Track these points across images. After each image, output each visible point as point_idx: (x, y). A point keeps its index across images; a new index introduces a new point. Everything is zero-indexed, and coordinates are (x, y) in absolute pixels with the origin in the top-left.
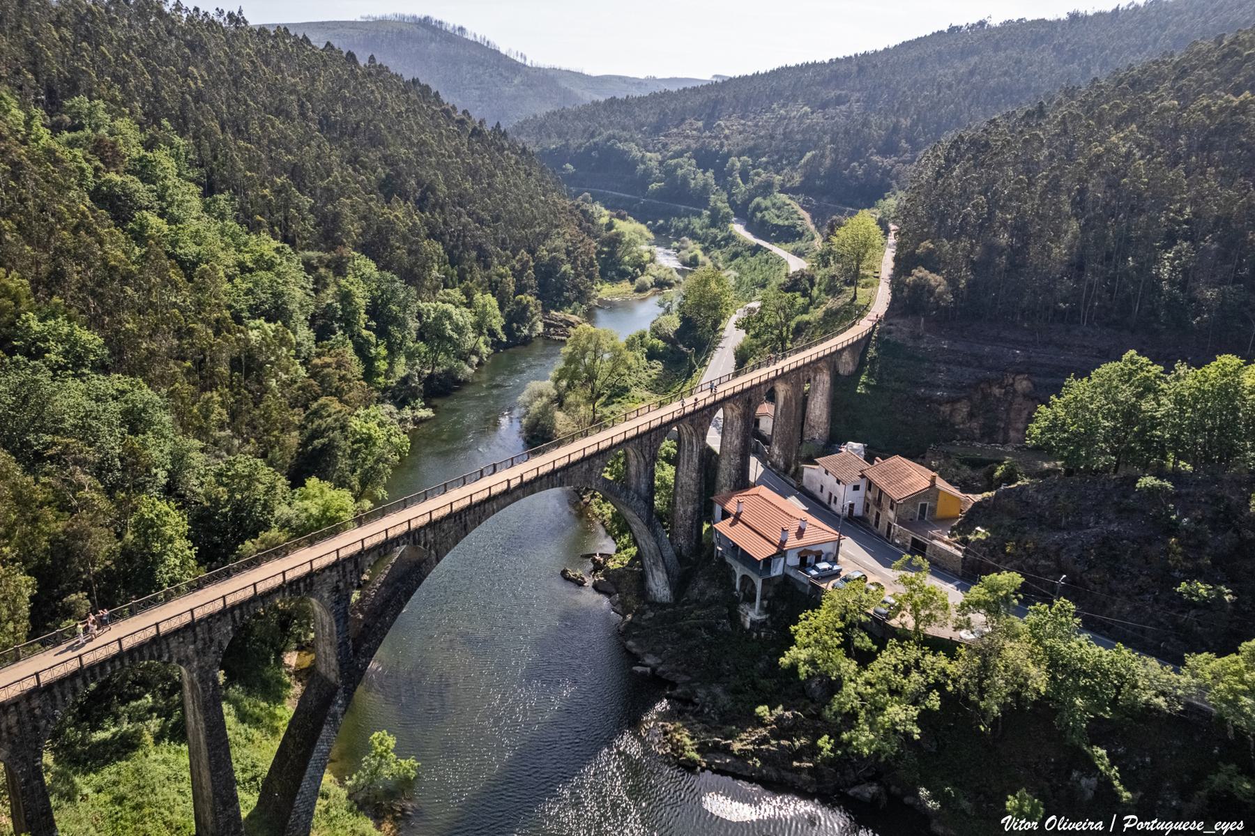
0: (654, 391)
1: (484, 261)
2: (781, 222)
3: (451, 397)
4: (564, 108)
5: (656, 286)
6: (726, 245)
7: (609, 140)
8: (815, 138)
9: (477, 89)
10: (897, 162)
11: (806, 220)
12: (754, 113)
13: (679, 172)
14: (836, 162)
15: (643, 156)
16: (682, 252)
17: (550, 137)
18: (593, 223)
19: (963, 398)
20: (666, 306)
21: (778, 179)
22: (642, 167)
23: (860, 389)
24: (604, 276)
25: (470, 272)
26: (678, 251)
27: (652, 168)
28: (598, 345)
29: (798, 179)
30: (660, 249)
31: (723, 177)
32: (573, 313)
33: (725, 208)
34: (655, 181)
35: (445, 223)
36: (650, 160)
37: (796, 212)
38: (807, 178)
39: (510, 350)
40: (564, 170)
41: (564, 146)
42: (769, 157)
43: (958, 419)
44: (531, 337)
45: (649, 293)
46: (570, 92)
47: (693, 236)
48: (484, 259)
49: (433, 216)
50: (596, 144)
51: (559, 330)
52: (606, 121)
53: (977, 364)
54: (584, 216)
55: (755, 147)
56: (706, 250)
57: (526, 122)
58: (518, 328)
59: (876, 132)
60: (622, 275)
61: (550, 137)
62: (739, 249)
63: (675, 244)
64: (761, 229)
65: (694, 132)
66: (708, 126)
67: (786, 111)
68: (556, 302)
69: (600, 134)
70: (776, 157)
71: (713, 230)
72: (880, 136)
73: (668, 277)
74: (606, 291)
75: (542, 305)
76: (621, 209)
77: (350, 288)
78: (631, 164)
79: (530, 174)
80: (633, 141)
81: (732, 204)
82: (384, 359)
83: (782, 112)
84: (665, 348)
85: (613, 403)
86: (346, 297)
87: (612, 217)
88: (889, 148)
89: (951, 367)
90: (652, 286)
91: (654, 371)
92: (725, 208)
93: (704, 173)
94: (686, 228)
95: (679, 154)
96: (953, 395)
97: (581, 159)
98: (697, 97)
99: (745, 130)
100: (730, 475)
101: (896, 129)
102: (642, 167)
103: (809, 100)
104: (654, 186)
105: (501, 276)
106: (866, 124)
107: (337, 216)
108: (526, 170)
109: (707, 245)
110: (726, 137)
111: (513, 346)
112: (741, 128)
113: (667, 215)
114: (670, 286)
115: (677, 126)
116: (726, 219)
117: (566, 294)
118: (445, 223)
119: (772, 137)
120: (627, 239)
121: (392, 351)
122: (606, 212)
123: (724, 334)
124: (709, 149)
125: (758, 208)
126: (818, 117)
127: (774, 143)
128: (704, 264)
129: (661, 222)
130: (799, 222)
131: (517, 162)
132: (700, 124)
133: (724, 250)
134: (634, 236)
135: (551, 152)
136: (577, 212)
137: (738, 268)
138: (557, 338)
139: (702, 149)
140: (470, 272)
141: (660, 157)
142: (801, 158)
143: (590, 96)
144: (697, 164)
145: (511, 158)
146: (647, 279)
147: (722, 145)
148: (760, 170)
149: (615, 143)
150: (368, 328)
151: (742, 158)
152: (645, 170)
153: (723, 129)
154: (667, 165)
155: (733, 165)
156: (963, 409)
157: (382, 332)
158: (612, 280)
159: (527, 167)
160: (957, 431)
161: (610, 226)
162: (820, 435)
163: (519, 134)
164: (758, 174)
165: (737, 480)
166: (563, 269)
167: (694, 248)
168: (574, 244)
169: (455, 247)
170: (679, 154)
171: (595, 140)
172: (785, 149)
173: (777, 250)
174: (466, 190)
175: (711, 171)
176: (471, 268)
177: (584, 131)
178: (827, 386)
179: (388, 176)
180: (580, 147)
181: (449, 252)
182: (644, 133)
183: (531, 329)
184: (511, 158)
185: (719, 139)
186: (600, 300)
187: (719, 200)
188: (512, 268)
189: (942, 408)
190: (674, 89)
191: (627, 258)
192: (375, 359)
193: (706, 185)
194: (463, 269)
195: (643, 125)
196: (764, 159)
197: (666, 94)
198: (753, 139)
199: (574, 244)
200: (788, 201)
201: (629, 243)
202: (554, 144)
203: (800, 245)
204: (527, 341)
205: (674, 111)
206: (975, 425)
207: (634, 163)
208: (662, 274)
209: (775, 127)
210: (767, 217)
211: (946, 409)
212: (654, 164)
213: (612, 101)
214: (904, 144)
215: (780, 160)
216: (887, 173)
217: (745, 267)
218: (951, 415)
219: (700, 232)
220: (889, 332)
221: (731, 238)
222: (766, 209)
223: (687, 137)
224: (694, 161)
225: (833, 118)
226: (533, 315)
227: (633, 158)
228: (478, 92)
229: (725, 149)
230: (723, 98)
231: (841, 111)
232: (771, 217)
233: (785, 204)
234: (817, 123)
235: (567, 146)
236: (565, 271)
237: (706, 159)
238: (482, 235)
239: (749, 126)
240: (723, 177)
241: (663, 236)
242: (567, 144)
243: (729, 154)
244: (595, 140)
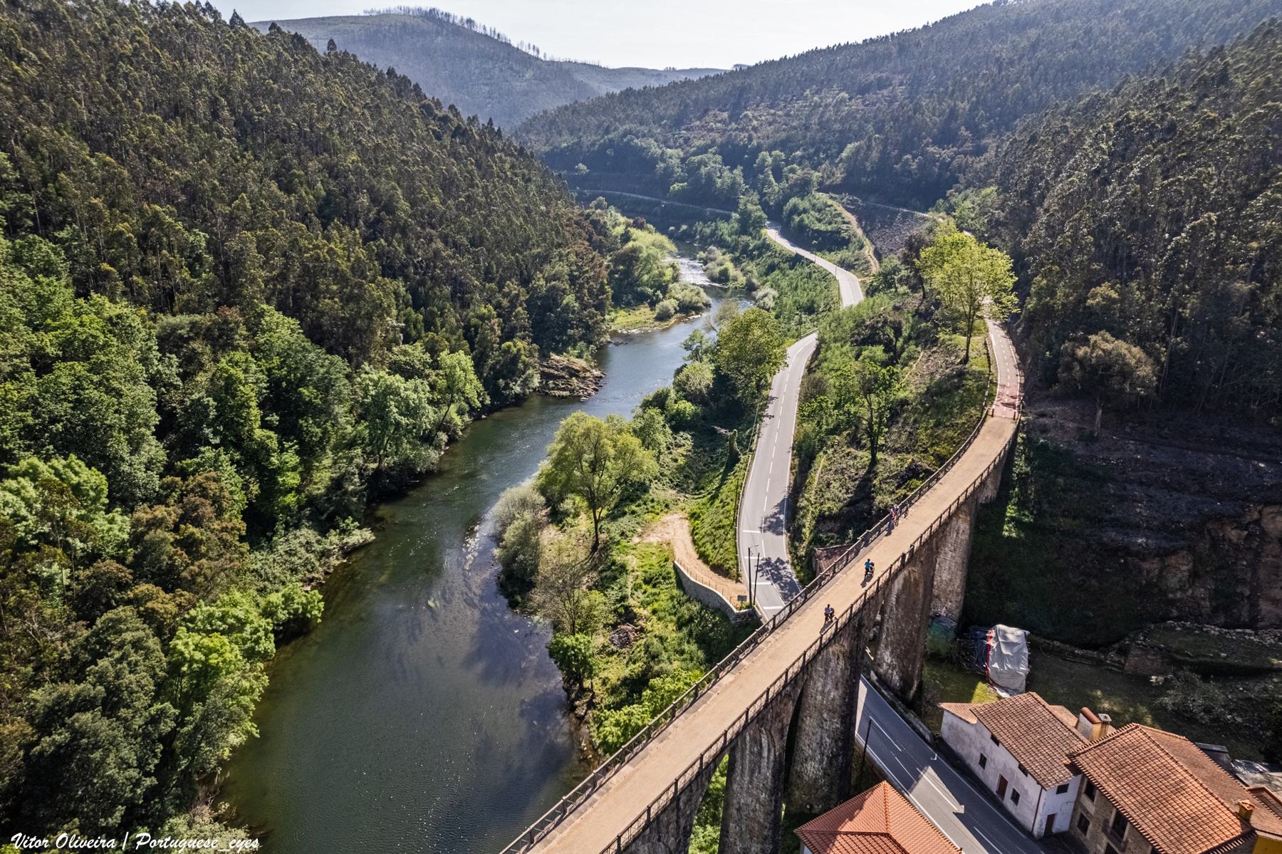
0: (680, 487)
1: (461, 299)
2: (822, 227)
3: (405, 501)
4: (576, 102)
5: (680, 311)
6: (760, 255)
7: (625, 135)
8: (855, 127)
9: (487, 85)
10: (957, 153)
11: (854, 227)
12: (785, 101)
13: (703, 170)
14: (884, 154)
15: (663, 153)
16: (710, 265)
17: (560, 135)
18: (605, 235)
19: (1182, 549)
20: (694, 347)
21: (816, 176)
22: (662, 165)
23: (1008, 531)
24: (618, 302)
25: (441, 315)
26: (705, 263)
27: (673, 167)
28: (597, 447)
29: (839, 176)
30: (685, 260)
31: (752, 174)
32: (580, 356)
33: (757, 211)
34: (677, 181)
35: (408, 250)
36: (671, 157)
37: (839, 215)
38: (850, 173)
39: (497, 415)
41: (576, 144)
42: (804, 150)
43: (1173, 582)
44: (524, 394)
45: (673, 320)
46: (585, 85)
47: (721, 244)
48: (461, 296)
49: (390, 244)
50: (611, 140)
51: (560, 382)
52: (622, 116)
53: (1197, 487)
54: (595, 228)
55: (788, 139)
56: (736, 261)
57: (535, 118)
58: (507, 384)
59: (930, 118)
60: (641, 298)
61: (560, 135)
62: (776, 261)
63: (702, 254)
64: (799, 235)
65: (719, 125)
66: (734, 117)
67: (821, 98)
68: (558, 342)
69: (616, 129)
70: (812, 150)
71: (746, 238)
72: (935, 124)
73: (695, 299)
74: (621, 320)
75: (539, 351)
76: (640, 214)
77: (232, 371)
79: (529, 180)
80: (652, 137)
81: (765, 205)
82: (294, 469)
83: (816, 98)
84: (695, 415)
85: (624, 514)
86: (226, 389)
87: (628, 225)
88: (946, 137)
89: (1152, 491)
90: (676, 312)
91: (681, 450)
92: (757, 211)
93: (731, 170)
94: (713, 234)
95: (703, 150)
96: (1164, 544)
97: (596, 158)
98: (721, 85)
99: (774, 121)
100: (821, 744)
101: (953, 114)
102: (662, 165)
103: (845, 85)
105: (482, 318)
106: (917, 109)
107: (240, 257)
108: (524, 175)
109: (737, 254)
110: (755, 129)
111: (499, 409)
112: (770, 118)
113: (691, 218)
114: (698, 310)
115: (700, 119)
116: (758, 224)
117: (570, 332)
118: (408, 250)
119: (807, 128)
120: (644, 254)
121: (309, 453)
122: (622, 219)
123: (772, 393)
124: (736, 142)
125: (795, 210)
126: (856, 104)
127: (809, 134)
128: (735, 280)
129: (684, 227)
130: (844, 227)
131: (513, 167)
132: (725, 115)
134: (653, 251)
135: (563, 151)
136: (586, 223)
137: (775, 285)
138: (557, 393)
139: (728, 142)
140: (441, 315)
141: (682, 154)
142: (841, 151)
143: (604, 89)
144: (723, 160)
145: (505, 162)
146: (670, 304)
147: (750, 139)
148: (795, 166)
149: (632, 140)
150: (265, 425)
151: (773, 153)
152: (665, 169)
153: (751, 120)
154: (690, 163)
155: (764, 160)
156: (1182, 566)
157: (287, 430)
158: (629, 306)
159: (526, 172)
160: (1173, 602)
161: (626, 238)
162: (949, 610)
163: (528, 132)
164: (793, 171)
165: (835, 756)
166: (565, 302)
167: (723, 260)
168: (580, 268)
169: (422, 283)
170: (703, 150)
171: (610, 136)
172: (822, 141)
173: (822, 262)
174: (434, 206)
175: (740, 168)
176: (442, 309)
177: (599, 127)
178: (964, 537)
179: (329, 192)
180: (593, 144)
181: (412, 290)
182: (664, 127)
183: (525, 384)
184: (505, 162)
185: (747, 131)
186: (614, 334)
187: (750, 203)
188: (498, 306)
189: (1146, 565)
190: (695, 78)
191: (646, 278)
192: (279, 471)
193: (734, 183)
194: (432, 313)
195: (662, 118)
196: (798, 153)
197: (687, 83)
198: (784, 130)
199: (580, 268)
200: (830, 202)
201: (647, 259)
202: (565, 141)
203: (844, 254)
204: (519, 400)
205: (696, 102)
206: (1200, 592)
207: (653, 162)
208: (687, 296)
209: (809, 117)
210: (807, 222)
211: (1152, 566)
212: (675, 161)
213: (628, 93)
214: (964, 132)
215: (817, 153)
216: (945, 166)
217: (784, 284)
218: (1160, 576)
219: (729, 239)
220: (1044, 430)
221: (765, 247)
222: (805, 211)
223: (712, 130)
224: (719, 158)
225: (874, 104)
226: (526, 366)
227: (652, 155)
228: (487, 88)
229: (755, 142)
230: (750, 85)
231: (883, 96)
232: (810, 220)
233: (827, 206)
234: (857, 111)
236: (567, 304)
237: (733, 155)
238: (463, 265)
239: (780, 116)
240: (752, 174)
241: (686, 244)
243: (759, 149)
244: (610, 136)
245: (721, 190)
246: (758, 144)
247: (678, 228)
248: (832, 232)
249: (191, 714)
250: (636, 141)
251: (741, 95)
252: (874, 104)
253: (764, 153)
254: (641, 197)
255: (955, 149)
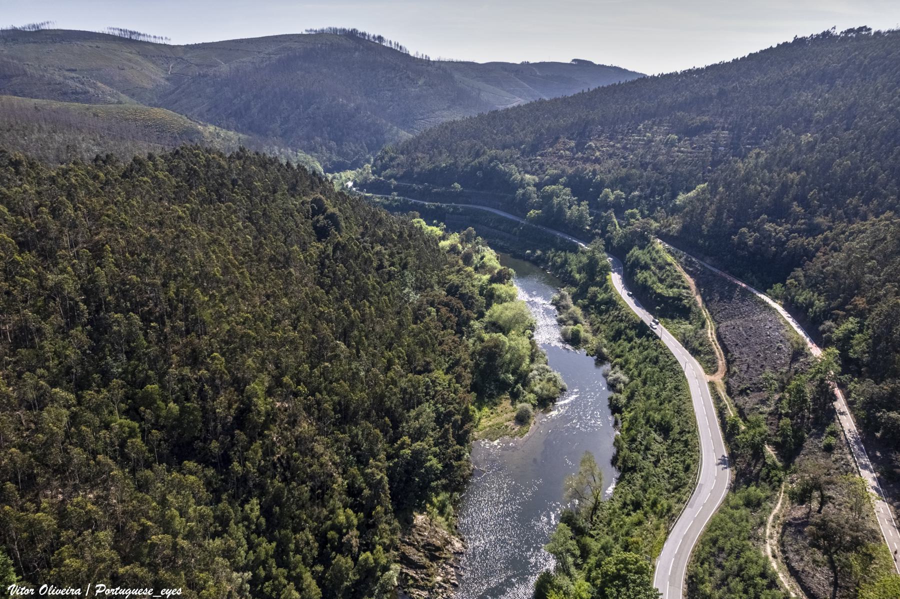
7: (491, 161)
9: (389, 90)
40: (453, 188)
42: (642, 190)
50: (480, 163)
65: (567, 152)
66: (580, 147)
70: (648, 191)
78: (511, 186)
80: (513, 162)
88: (778, 212)
95: (554, 180)
97: (467, 178)
104: (532, 213)
132: (573, 144)
133: (604, 317)
135: (442, 170)
152: (524, 194)
170: (554, 180)
172: (657, 182)
180: (466, 165)
202: (444, 161)
214: (796, 208)
215: (652, 194)
227: (514, 180)
235: (454, 164)
239: (618, 149)
242: (456, 162)
245: (570, 221)
246: (601, 179)
247: (534, 252)
248: (674, 299)
249: (149, 427)
250: (500, 166)
251: (585, 127)
252: (701, 148)
253: (607, 190)
254: (503, 214)
255: (789, 226)
